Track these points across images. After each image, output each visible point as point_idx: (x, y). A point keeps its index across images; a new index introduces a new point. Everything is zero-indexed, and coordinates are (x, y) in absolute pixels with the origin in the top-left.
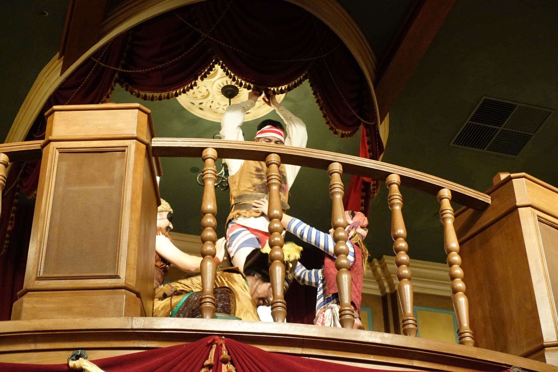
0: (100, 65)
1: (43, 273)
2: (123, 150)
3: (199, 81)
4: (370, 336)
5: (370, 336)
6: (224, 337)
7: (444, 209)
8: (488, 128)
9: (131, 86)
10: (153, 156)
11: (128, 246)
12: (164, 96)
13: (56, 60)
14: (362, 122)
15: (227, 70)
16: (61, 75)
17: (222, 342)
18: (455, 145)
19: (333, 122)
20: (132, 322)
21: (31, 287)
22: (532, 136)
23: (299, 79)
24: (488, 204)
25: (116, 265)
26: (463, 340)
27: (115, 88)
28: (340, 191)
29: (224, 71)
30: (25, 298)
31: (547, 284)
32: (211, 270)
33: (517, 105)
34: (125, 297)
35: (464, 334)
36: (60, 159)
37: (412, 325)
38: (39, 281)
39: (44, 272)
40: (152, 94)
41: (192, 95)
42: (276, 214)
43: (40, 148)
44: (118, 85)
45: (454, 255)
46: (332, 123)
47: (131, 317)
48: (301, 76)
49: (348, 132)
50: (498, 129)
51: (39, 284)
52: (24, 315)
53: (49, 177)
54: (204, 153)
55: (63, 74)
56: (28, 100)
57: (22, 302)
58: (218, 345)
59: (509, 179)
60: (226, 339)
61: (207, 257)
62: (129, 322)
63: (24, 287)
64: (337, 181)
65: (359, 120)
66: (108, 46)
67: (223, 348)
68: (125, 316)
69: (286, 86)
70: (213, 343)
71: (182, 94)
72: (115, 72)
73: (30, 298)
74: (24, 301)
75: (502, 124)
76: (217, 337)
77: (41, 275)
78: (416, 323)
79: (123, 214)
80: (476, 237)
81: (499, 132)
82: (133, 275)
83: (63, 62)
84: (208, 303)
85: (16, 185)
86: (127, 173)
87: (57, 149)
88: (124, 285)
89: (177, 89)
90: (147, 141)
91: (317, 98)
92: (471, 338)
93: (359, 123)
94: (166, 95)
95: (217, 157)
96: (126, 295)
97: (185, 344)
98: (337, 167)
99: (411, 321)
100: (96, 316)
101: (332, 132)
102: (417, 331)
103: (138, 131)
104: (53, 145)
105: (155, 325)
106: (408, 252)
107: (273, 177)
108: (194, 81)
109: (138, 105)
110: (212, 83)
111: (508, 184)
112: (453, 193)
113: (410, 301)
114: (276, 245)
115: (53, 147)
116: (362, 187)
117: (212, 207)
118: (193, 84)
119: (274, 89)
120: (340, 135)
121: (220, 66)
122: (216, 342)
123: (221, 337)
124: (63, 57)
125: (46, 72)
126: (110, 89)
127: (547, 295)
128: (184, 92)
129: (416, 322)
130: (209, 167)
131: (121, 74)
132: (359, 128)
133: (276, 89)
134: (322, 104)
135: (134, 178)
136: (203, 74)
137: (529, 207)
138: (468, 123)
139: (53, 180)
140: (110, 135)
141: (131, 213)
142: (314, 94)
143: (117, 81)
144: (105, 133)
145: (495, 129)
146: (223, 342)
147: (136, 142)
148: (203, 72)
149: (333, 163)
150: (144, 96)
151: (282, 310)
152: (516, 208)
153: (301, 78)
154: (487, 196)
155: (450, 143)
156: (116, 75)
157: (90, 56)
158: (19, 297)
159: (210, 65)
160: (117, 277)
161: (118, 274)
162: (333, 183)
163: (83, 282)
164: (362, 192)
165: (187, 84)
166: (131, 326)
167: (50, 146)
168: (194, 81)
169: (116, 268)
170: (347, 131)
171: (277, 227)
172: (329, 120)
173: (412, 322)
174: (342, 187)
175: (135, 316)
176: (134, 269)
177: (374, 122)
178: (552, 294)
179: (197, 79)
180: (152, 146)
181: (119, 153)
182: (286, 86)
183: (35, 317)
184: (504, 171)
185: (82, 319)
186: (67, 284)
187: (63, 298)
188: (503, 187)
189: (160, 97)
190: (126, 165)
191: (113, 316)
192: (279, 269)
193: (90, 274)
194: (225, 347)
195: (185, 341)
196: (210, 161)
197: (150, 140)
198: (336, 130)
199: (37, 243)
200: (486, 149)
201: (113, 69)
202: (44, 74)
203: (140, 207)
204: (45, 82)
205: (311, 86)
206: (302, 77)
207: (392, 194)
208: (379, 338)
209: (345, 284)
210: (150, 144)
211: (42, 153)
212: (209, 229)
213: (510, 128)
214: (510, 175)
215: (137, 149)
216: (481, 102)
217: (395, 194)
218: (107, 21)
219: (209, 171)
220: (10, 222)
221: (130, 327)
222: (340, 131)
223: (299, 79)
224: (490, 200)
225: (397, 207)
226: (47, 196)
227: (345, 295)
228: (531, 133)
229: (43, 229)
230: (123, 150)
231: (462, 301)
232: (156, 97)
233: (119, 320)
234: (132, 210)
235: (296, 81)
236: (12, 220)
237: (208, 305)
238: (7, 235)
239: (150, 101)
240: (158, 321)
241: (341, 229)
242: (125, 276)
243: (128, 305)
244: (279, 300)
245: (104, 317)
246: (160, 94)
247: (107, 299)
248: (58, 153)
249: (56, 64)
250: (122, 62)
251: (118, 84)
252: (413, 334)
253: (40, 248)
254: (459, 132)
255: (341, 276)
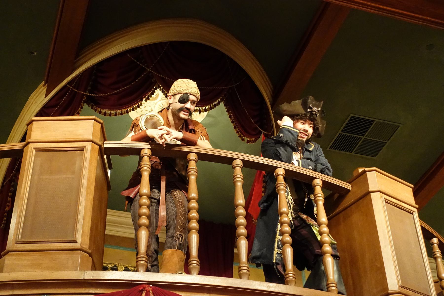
0: (73, 90)
1: (21, 238)
2: (82, 150)
3: (143, 102)
4: (259, 285)
5: (259, 285)
6: (151, 286)
7: (317, 193)
8: (346, 135)
9: (95, 105)
10: (105, 154)
11: (84, 219)
12: (119, 113)
13: (42, 86)
14: (262, 132)
15: (166, 93)
16: (45, 97)
17: (150, 289)
18: (330, 150)
19: (241, 132)
20: (84, 274)
21: (11, 249)
22: (386, 143)
23: (218, 101)
24: (349, 191)
25: (75, 233)
26: (330, 289)
27: (83, 107)
28: (240, 180)
29: (164, 95)
30: (6, 257)
31: (392, 248)
32: (145, 237)
33: (375, 121)
34: (80, 256)
35: (330, 284)
36: (36, 156)
37: (292, 278)
38: (18, 244)
39: (22, 238)
40: (110, 111)
41: (140, 112)
42: (194, 196)
43: (22, 148)
44: (86, 106)
45: (323, 227)
46: (241, 133)
47: (83, 271)
48: (219, 99)
49: (252, 139)
50: (362, 138)
51: (17, 247)
52: (5, 269)
53: (27, 168)
54: (142, 152)
55: (47, 97)
56: (23, 114)
57: (5, 260)
58: (147, 291)
59: (364, 172)
60: (154, 287)
61: (142, 228)
62: (82, 274)
63: (6, 249)
64: (238, 172)
65: (260, 131)
66: (79, 76)
67: (150, 294)
68: (79, 270)
69: (209, 106)
70: (143, 290)
71: (132, 111)
72: (84, 95)
73: (11, 257)
74: (6, 259)
75: (365, 135)
76: (147, 286)
77: (19, 240)
78: (294, 277)
79: (81, 195)
80: (341, 214)
81: (362, 139)
82: (87, 240)
83: (47, 88)
84: (142, 261)
85: (12, 177)
86: (84, 166)
87: (34, 148)
88: (80, 247)
89: (128, 108)
90: (100, 143)
91: (230, 115)
92: (335, 287)
93: (260, 133)
94: (114, 113)
95: (151, 155)
96: (81, 254)
97: (123, 291)
98: (238, 163)
99: (292, 275)
100: (58, 270)
101: (240, 139)
102: (249, 275)
103: (93, 135)
104: (31, 145)
105: (100, 276)
106: (198, 210)
107: (192, 170)
108: (140, 102)
109: (93, 117)
110: (155, 104)
111: (364, 175)
112: (324, 182)
113: (291, 260)
114: (193, 219)
115: (31, 147)
116: (263, 179)
117: (147, 191)
118: (139, 103)
119: (200, 108)
120: (246, 141)
121: (161, 91)
122: (146, 289)
123: (149, 285)
124: (47, 85)
125: (34, 95)
126: (80, 108)
127: (391, 256)
128: (133, 110)
129: (295, 275)
130: (145, 162)
131: (87, 96)
132: (260, 136)
133: (201, 109)
134: (233, 119)
135: (89, 170)
136: (147, 97)
137: (379, 193)
138: (340, 134)
139: (30, 171)
140: (73, 139)
141: (87, 196)
142: (227, 111)
143: (85, 102)
144: (391, 193)
145: (360, 138)
146: (151, 289)
147: (92, 144)
148: (147, 96)
149: (236, 160)
150: (104, 112)
151: (196, 266)
152: (369, 193)
153: (219, 100)
154: (348, 184)
155: (327, 148)
156: (85, 98)
157: (66, 84)
158: (2, 257)
159: (152, 91)
160: (75, 241)
161: (76, 240)
162: (236, 174)
163: (50, 245)
164: (263, 183)
165: (135, 104)
166: (83, 277)
167: (29, 146)
168: (140, 102)
169: (74, 235)
170: (250, 138)
171: (194, 205)
172: (238, 130)
173: (292, 276)
174: (242, 177)
175: (87, 270)
176: (87, 236)
177: (271, 132)
178: (395, 256)
179: (142, 100)
180: (104, 147)
181: (80, 152)
182: (209, 106)
183: (13, 270)
184: (361, 167)
185: (47, 272)
186: (38, 247)
187: (34, 257)
188: (359, 178)
189: (105, 113)
190: (84, 160)
191: (71, 270)
192: (195, 236)
193: (64, 239)
194: (152, 293)
195: (122, 289)
196: (146, 159)
197: (103, 143)
198: (243, 138)
199: (17, 216)
200: (354, 151)
201: (82, 93)
202: (34, 96)
203: (93, 191)
204: (34, 103)
205: (225, 106)
206: (220, 99)
207: (279, 183)
208: (266, 286)
209: (243, 247)
210: (102, 146)
211: (23, 151)
212: (144, 207)
213: (370, 138)
214: (365, 169)
215: (92, 148)
216: (349, 118)
217: (280, 182)
218: (78, 58)
219: (146, 165)
220: (7, 204)
221: (83, 278)
222: (246, 139)
223: (218, 101)
224: (351, 187)
225: (282, 191)
226: (26, 183)
227: (243, 256)
228: (386, 141)
229: (22, 207)
230: (82, 150)
231: (329, 260)
232: (113, 113)
233: (75, 273)
234: (87, 193)
235: (216, 103)
236: (9, 203)
237: (142, 262)
238: (5, 214)
239: (109, 116)
240: (103, 273)
241: (241, 208)
242: (80, 241)
243: (82, 262)
244: (194, 259)
245: (65, 271)
246: (116, 112)
247: (67, 258)
248: (34, 151)
249: (42, 89)
250: (89, 88)
251: (86, 104)
252: (246, 277)
253: (19, 220)
254: (334, 140)
255: (240, 241)
